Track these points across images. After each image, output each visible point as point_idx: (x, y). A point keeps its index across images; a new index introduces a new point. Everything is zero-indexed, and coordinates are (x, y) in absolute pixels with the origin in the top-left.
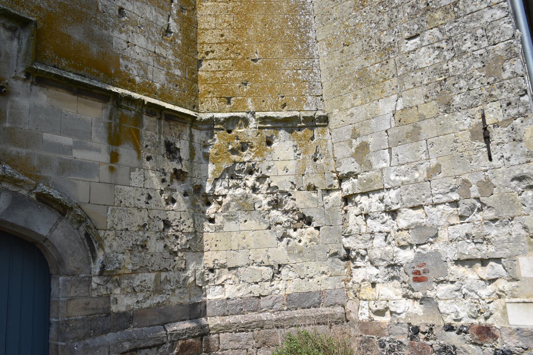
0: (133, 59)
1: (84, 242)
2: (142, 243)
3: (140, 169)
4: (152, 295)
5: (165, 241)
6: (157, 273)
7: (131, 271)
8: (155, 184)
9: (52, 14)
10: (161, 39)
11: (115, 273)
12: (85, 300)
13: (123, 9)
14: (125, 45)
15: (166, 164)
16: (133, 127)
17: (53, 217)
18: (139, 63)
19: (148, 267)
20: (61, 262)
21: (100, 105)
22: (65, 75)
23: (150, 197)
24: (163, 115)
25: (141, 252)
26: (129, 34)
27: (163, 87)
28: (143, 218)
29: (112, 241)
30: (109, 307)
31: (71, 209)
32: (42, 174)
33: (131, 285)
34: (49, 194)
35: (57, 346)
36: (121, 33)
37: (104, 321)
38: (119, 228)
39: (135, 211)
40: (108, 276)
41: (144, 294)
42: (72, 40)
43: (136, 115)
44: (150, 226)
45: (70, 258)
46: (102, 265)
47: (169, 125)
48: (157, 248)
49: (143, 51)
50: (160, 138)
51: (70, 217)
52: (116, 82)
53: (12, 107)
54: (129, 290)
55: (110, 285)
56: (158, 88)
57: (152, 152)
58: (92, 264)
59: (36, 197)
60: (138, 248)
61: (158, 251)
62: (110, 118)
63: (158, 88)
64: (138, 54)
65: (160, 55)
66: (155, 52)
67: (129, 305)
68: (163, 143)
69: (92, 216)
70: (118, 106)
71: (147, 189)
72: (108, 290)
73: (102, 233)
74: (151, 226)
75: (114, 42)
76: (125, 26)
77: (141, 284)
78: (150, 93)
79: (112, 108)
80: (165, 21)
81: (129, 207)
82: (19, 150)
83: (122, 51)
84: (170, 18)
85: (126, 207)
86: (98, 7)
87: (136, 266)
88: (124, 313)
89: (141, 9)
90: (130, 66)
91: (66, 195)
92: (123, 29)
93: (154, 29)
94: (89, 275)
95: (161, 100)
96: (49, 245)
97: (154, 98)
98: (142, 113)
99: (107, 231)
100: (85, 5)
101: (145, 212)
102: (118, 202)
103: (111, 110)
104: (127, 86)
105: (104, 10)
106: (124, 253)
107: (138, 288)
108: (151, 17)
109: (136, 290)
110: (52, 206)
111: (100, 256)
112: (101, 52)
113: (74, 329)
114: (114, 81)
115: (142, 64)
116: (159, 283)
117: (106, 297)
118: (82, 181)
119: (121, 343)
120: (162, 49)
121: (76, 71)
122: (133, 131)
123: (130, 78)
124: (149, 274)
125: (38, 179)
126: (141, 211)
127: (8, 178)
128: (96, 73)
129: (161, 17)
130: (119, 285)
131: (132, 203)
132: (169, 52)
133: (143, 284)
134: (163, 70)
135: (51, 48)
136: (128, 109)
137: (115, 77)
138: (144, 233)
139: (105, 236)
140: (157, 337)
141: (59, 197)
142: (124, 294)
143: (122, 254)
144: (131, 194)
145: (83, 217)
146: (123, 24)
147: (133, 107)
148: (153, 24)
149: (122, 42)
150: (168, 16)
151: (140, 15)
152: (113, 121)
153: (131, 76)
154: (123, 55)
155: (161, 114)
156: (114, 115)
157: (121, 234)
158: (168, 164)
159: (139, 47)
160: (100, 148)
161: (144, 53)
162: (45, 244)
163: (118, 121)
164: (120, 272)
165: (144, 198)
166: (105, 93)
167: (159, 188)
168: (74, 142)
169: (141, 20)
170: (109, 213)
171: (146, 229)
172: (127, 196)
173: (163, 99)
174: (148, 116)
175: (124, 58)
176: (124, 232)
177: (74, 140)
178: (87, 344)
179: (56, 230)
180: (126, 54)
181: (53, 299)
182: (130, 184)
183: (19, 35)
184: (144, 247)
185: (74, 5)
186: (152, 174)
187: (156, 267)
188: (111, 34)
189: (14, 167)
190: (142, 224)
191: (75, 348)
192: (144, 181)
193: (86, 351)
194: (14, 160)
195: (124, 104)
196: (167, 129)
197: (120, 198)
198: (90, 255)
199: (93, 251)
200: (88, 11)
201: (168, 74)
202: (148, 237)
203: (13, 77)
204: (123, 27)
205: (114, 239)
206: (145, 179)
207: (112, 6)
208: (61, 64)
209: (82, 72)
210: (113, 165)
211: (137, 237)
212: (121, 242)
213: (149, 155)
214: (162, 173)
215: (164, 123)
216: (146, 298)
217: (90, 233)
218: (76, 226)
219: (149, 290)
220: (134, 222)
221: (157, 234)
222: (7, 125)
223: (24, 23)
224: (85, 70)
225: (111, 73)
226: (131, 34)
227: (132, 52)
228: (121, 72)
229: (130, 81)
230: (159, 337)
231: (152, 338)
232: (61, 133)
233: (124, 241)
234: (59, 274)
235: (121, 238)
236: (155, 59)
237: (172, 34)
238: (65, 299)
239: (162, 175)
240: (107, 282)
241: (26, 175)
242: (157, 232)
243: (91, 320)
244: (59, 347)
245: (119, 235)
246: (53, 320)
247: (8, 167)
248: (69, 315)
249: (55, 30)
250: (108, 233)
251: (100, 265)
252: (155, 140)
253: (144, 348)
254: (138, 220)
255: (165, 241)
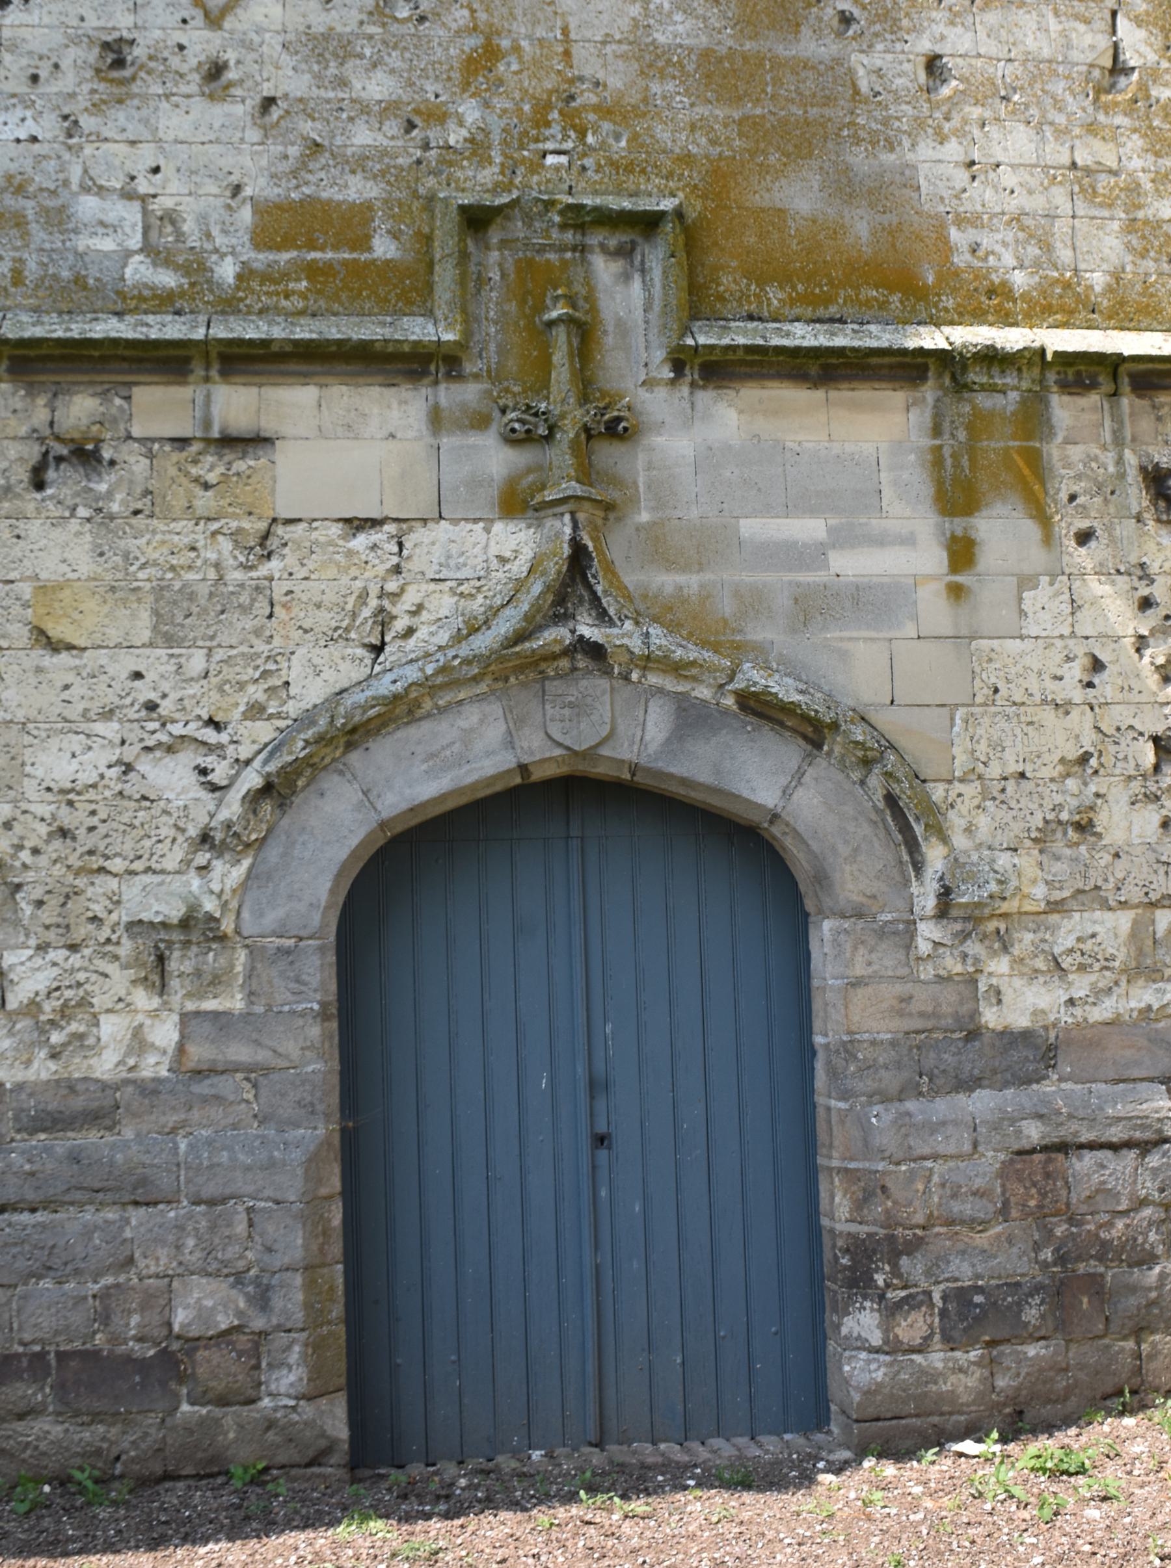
0: (995, 215)
1: (884, 820)
2: (1077, 818)
3: (1053, 577)
4: (1123, 983)
5: (1162, 806)
6: (1140, 911)
7: (1043, 905)
8: (1112, 620)
9: (722, 164)
10: (1090, 109)
11: (987, 911)
12: (899, 989)
13: (940, 57)
14: (961, 177)
15: (1151, 546)
16: (1017, 443)
17: (789, 752)
18: (1018, 220)
19: (1102, 893)
20: (822, 879)
21: (898, 397)
22: (776, 341)
23: (1097, 665)
24: (1126, 380)
25: (1077, 844)
26: (969, 137)
27: (1118, 279)
28: (1077, 736)
29: (974, 813)
30: (975, 1013)
31: (835, 726)
32: (749, 637)
33: (1047, 948)
34: (766, 692)
35: (828, 1109)
36: (941, 143)
37: (959, 1053)
38: (994, 771)
39: (1048, 716)
40: (966, 919)
41: (1093, 978)
42: (790, 222)
43: (1023, 402)
44: (1103, 759)
45: (847, 868)
46: (943, 886)
47: (1154, 407)
48: (1136, 830)
49: (1027, 177)
50: (1120, 461)
51: (837, 749)
52: (946, 310)
53: (650, 467)
54: (1040, 964)
55: (973, 947)
56: (1098, 289)
57: (1093, 514)
58: (914, 884)
59: (737, 702)
60: (1065, 833)
61: (1137, 841)
62: (937, 431)
63: (1098, 289)
64: (1012, 192)
65: (1095, 167)
66: (1074, 165)
67: (1043, 1012)
68: (1133, 475)
69: (901, 742)
70: (961, 387)
71: (1087, 638)
72: (970, 961)
73: (938, 792)
74: (1107, 760)
75: (922, 181)
76: (954, 114)
77: (1081, 946)
78: (1072, 312)
79: (938, 400)
80: (1100, 36)
81: (1023, 704)
82: (681, 579)
83: (955, 202)
84: (1119, 17)
85: (1015, 704)
86: (854, 85)
87: (1061, 889)
88: (1026, 1036)
89: (1003, 32)
90: (987, 241)
91: (820, 689)
92: (947, 126)
93: (1062, 84)
94: (906, 916)
95: (1114, 328)
96: (784, 834)
97: (1088, 328)
98: (1045, 388)
99: (956, 783)
100: (814, 95)
101: (1083, 713)
102: (986, 691)
103: (935, 407)
104: (985, 313)
105: (878, 88)
106: (1016, 850)
107: (1069, 959)
108: (1045, 44)
109: (1064, 966)
110: (781, 724)
111: (935, 856)
112: (884, 229)
113: (869, 1068)
114: (936, 306)
115: (1028, 221)
116: (1150, 943)
117: (965, 982)
118: (865, 639)
119: (1013, 1121)
120: (1097, 144)
121: (814, 311)
122: (1016, 457)
123: (992, 283)
124: (1110, 913)
125: (739, 650)
126: (1067, 713)
127: (658, 660)
128: (875, 299)
129: (1082, 27)
130: (1005, 949)
131: (1034, 688)
132: (1129, 144)
133: (1088, 946)
134: (1112, 219)
135: (734, 264)
136: (993, 389)
137: (938, 295)
138: (1085, 784)
139: (950, 800)
140: (1138, 1117)
141: (796, 698)
142: (1022, 975)
143: (1009, 853)
144: (1027, 661)
145: (872, 749)
146: (945, 109)
147: (1008, 380)
148: (1054, 66)
149: (950, 170)
150: (1108, 17)
151: (1001, 56)
152: (946, 441)
153: (994, 277)
154: (958, 214)
155: (1115, 377)
156: (948, 419)
157: (1003, 790)
158: (1159, 544)
159: (1012, 166)
160: (912, 533)
161: (1033, 182)
162: (776, 830)
163: (962, 435)
164: (1005, 907)
165: (1076, 671)
166: (908, 360)
167: (1131, 632)
168: (830, 530)
169: (1010, 67)
170: (956, 729)
171: (1090, 771)
172: (1013, 670)
173: (1122, 320)
174: (1070, 394)
175: (961, 221)
176: (1011, 786)
177: (830, 522)
178: (909, 1114)
179: (800, 789)
180: (969, 208)
181: (815, 983)
182: (1024, 631)
183: (643, 262)
184: (1084, 827)
185: (782, 109)
186: (1098, 587)
187: (1134, 894)
188: (910, 156)
189: (672, 627)
190: (1073, 754)
191: (874, 1120)
192: (1073, 614)
193: (903, 1130)
194: (671, 608)
195: (976, 376)
196: (1146, 424)
197: (993, 680)
198: (906, 858)
199: (913, 846)
200: (827, 112)
201: (1131, 226)
202: (1098, 795)
203: (644, 383)
204: (947, 119)
205: (978, 807)
206: (1075, 606)
207: (901, 63)
208: (769, 305)
209: (833, 310)
210: (959, 579)
211: (1058, 799)
212: (1002, 814)
213: (1084, 524)
214: (1140, 578)
215: (1131, 406)
216: (1100, 993)
217: (898, 791)
218: (856, 775)
219: (1111, 964)
220: (1045, 749)
221: (1133, 784)
222: (644, 517)
223: (649, 223)
224: (841, 301)
225: (925, 285)
226: (976, 132)
227: (989, 194)
228: (956, 274)
229: (991, 292)
230: (1147, 1117)
231: (1120, 1119)
232: (791, 509)
233: (1014, 813)
234: (823, 914)
235: (1003, 802)
236: (1076, 189)
237: (1135, 76)
238: (839, 982)
239: (1136, 584)
240: (964, 936)
241: (704, 644)
242: (1130, 778)
243: (919, 1048)
244: (834, 1113)
245: (996, 794)
246: (818, 1040)
247: (655, 631)
248: (854, 1028)
249: (738, 208)
250: (957, 791)
251: (935, 885)
252: (1102, 471)
253: (1092, 1146)
254: (1060, 741)
255: (1162, 806)
